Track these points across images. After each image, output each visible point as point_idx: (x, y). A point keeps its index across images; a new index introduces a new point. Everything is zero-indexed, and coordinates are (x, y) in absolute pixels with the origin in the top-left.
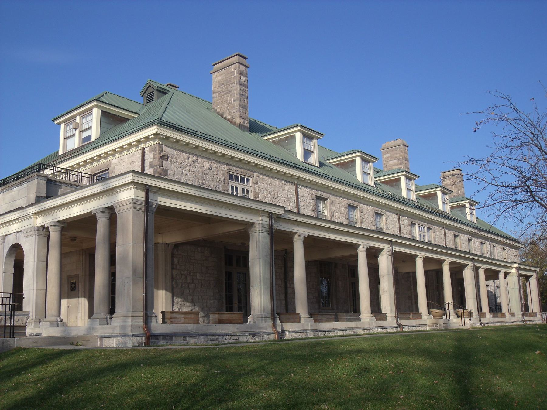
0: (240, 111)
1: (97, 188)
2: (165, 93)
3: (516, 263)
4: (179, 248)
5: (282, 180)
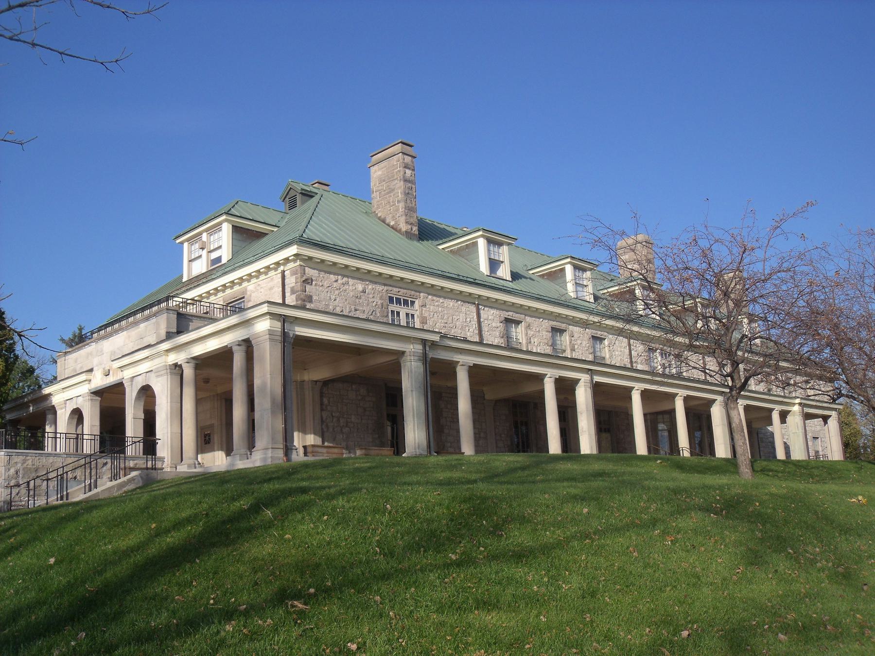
0: (406, 215)
1: (233, 320)
2: (312, 197)
3: (798, 397)
4: (330, 385)
5: (458, 300)
